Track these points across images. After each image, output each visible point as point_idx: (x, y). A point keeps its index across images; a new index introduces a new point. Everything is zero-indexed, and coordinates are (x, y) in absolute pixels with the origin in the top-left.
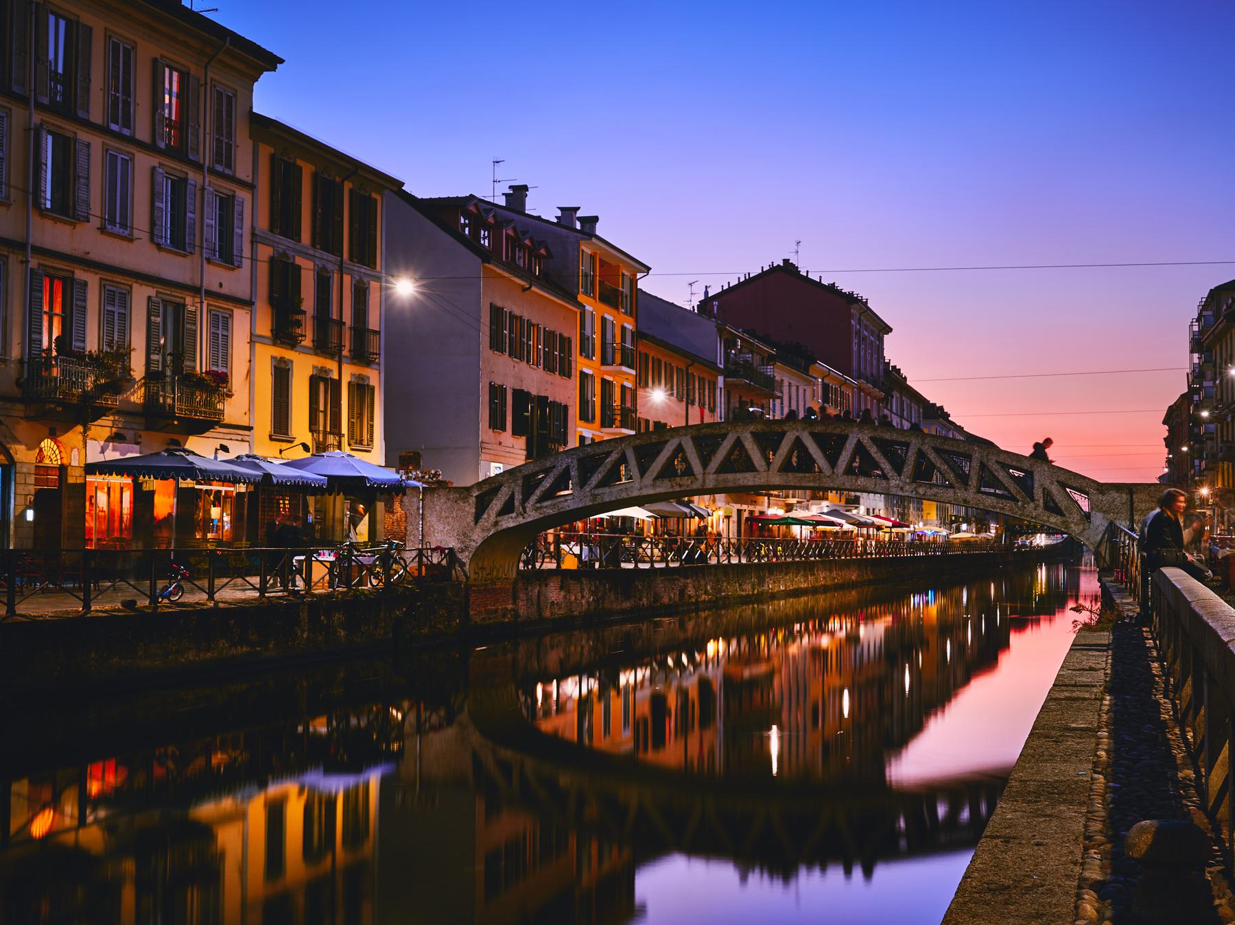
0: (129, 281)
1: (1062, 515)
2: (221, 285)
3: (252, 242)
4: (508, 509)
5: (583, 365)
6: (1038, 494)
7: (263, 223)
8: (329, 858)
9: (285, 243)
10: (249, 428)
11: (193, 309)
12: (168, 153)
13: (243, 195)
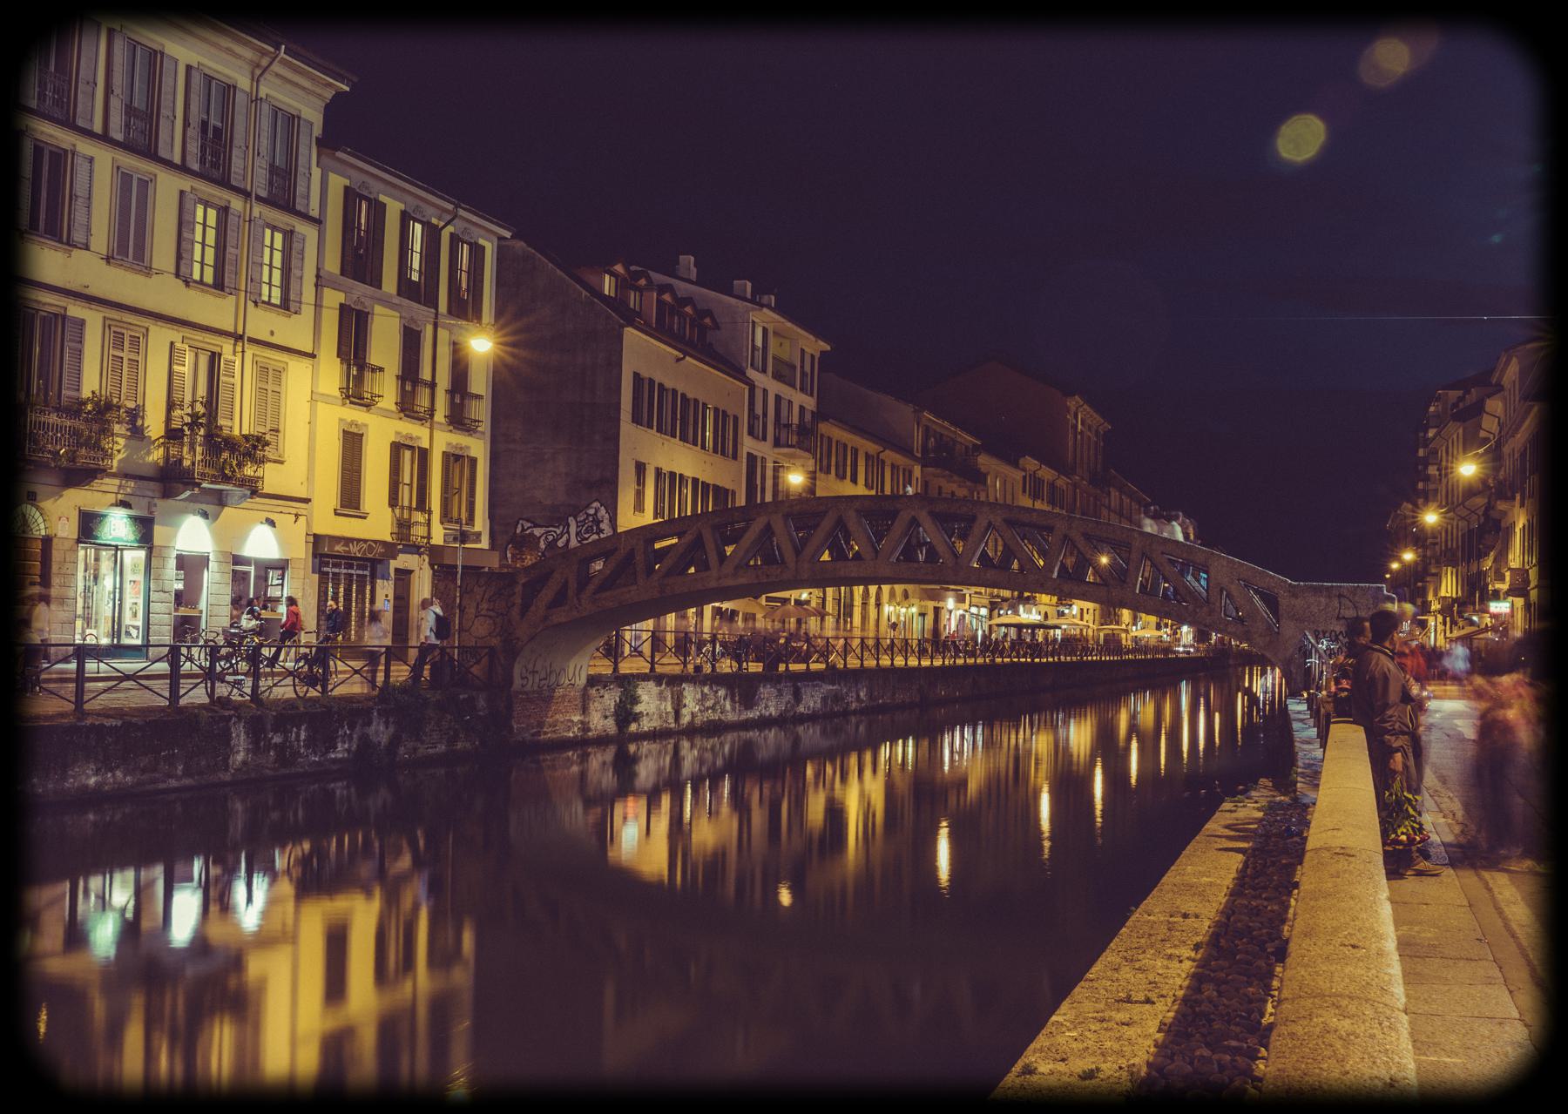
0: (284, 357)
2: (272, 333)
3: (316, 285)
4: (559, 600)
5: (748, 444)
7: (333, 265)
8: (408, 986)
9: (361, 289)
10: (307, 501)
11: (231, 357)
12: (127, 146)
13: (308, 232)
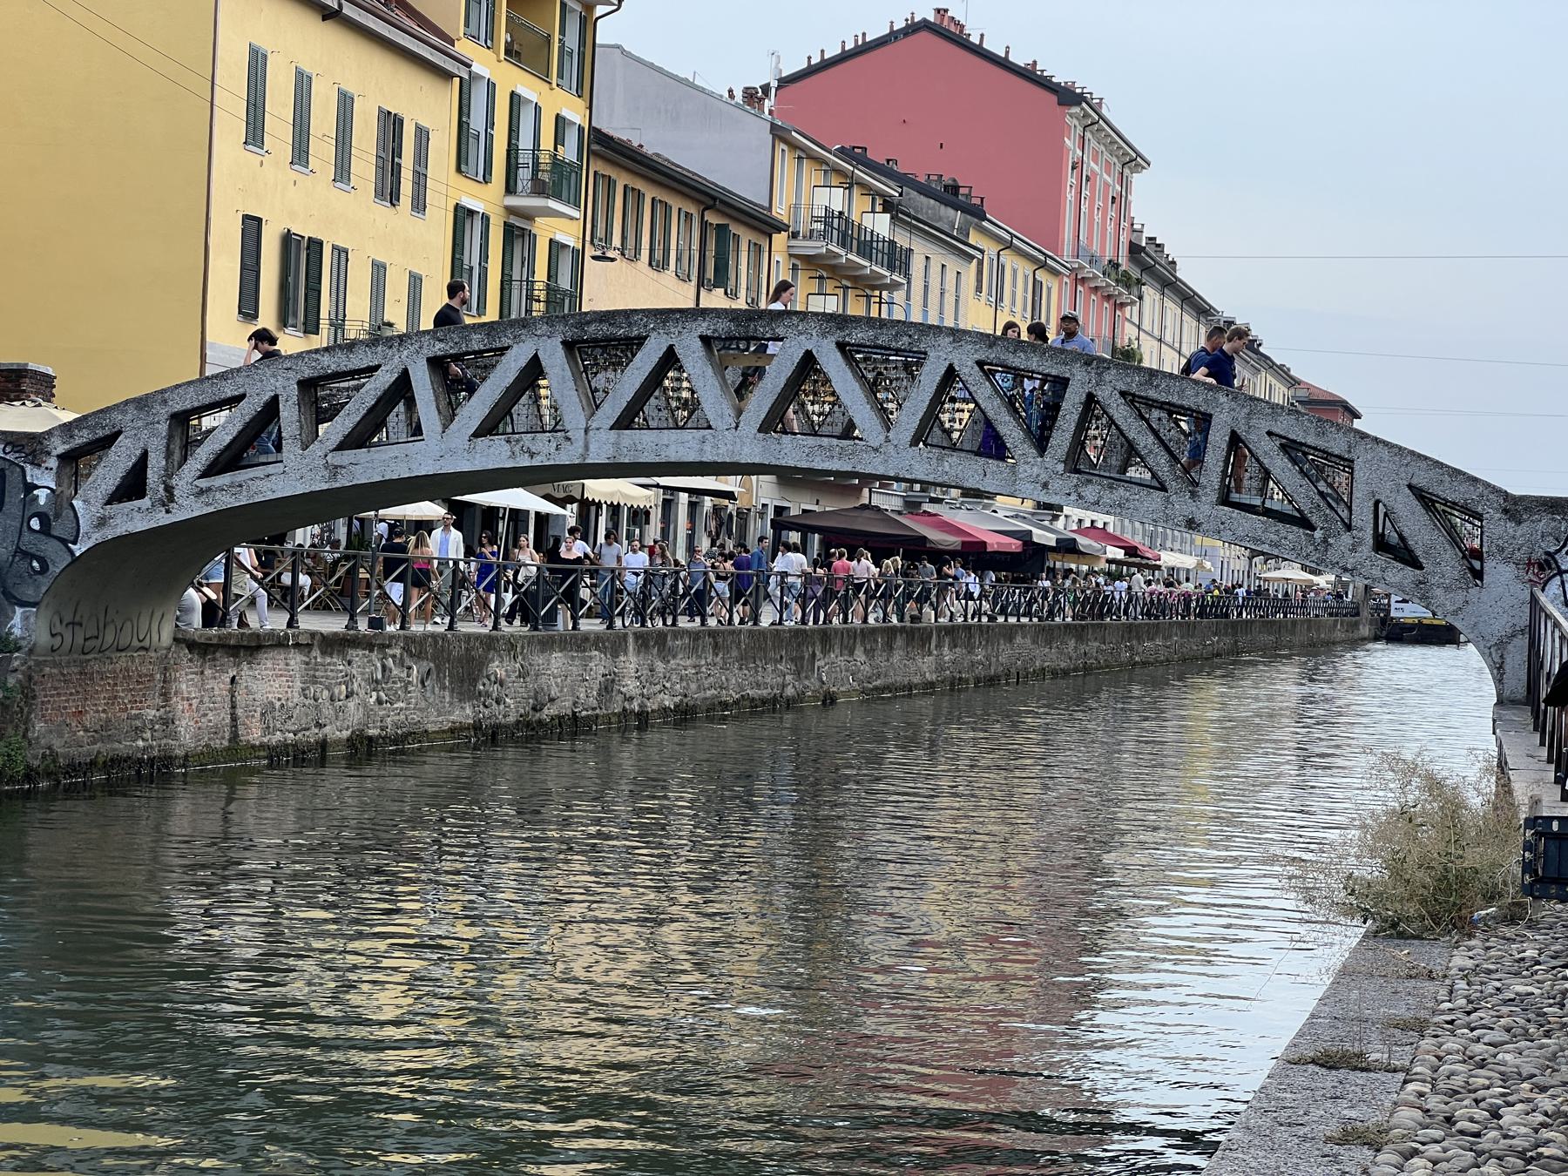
1: (1415, 563)
4: (132, 486)
6: (1362, 516)
